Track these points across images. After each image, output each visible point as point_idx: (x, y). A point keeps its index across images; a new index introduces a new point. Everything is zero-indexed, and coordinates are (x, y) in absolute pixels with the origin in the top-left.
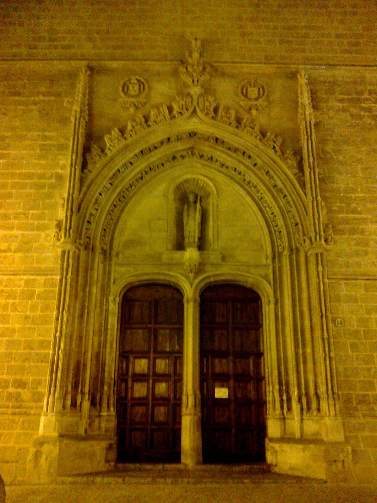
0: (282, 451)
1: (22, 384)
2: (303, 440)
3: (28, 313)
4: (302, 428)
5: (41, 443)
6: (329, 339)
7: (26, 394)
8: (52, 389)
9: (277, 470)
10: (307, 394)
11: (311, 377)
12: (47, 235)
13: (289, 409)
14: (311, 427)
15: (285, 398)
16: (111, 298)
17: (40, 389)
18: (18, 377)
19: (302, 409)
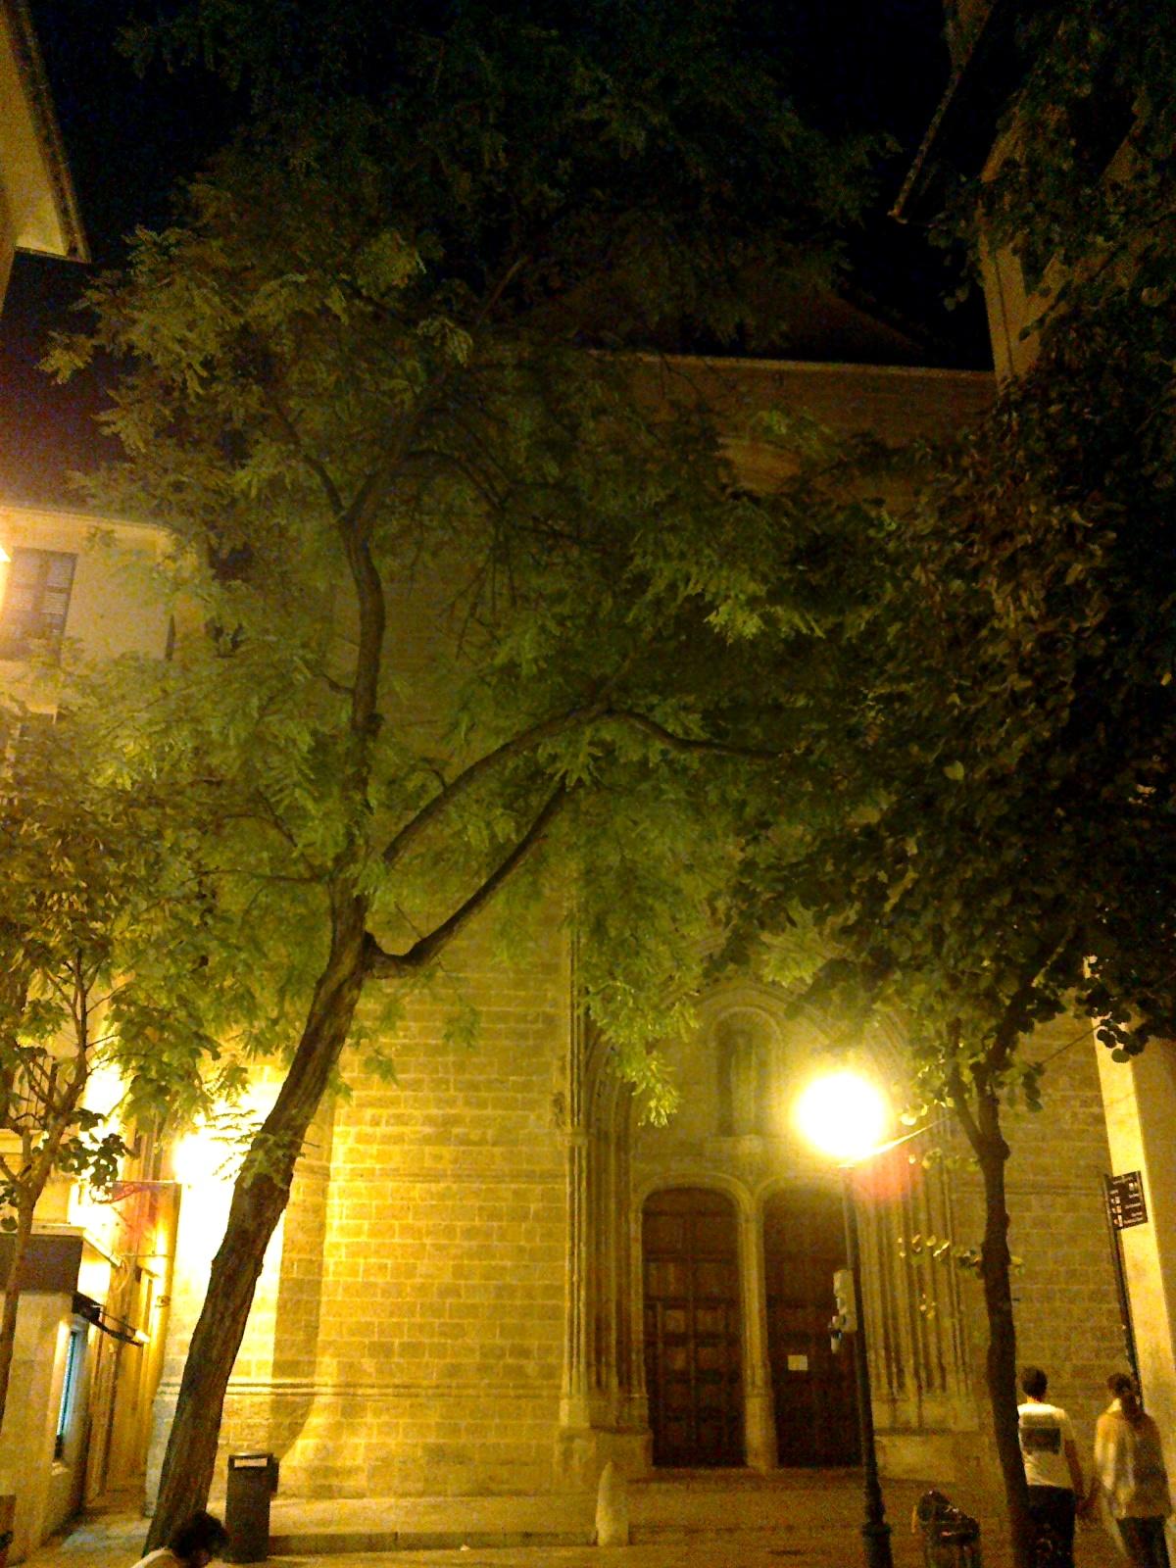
0: (895, 1446)
1: (525, 1353)
2: (923, 1430)
3: (522, 1243)
4: (920, 1416)
5: (569, 1437)
6: (958, 1286)
7: (531, 1367)
8: (575, 1360)
9: (886, 1474)
10: (927, 1365)
11: (932, 1339)
12: (539, 1117)
13: (901, 1386)
14: (933, 1411)
15: (894, 1370)
16: (632, 1216)
17: (552, 1360)
18: (517, 1341)
19: (920, 1387)
